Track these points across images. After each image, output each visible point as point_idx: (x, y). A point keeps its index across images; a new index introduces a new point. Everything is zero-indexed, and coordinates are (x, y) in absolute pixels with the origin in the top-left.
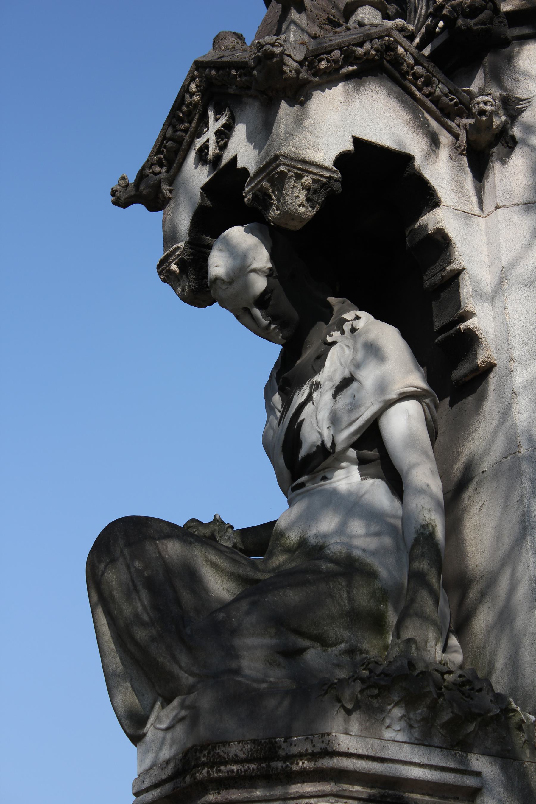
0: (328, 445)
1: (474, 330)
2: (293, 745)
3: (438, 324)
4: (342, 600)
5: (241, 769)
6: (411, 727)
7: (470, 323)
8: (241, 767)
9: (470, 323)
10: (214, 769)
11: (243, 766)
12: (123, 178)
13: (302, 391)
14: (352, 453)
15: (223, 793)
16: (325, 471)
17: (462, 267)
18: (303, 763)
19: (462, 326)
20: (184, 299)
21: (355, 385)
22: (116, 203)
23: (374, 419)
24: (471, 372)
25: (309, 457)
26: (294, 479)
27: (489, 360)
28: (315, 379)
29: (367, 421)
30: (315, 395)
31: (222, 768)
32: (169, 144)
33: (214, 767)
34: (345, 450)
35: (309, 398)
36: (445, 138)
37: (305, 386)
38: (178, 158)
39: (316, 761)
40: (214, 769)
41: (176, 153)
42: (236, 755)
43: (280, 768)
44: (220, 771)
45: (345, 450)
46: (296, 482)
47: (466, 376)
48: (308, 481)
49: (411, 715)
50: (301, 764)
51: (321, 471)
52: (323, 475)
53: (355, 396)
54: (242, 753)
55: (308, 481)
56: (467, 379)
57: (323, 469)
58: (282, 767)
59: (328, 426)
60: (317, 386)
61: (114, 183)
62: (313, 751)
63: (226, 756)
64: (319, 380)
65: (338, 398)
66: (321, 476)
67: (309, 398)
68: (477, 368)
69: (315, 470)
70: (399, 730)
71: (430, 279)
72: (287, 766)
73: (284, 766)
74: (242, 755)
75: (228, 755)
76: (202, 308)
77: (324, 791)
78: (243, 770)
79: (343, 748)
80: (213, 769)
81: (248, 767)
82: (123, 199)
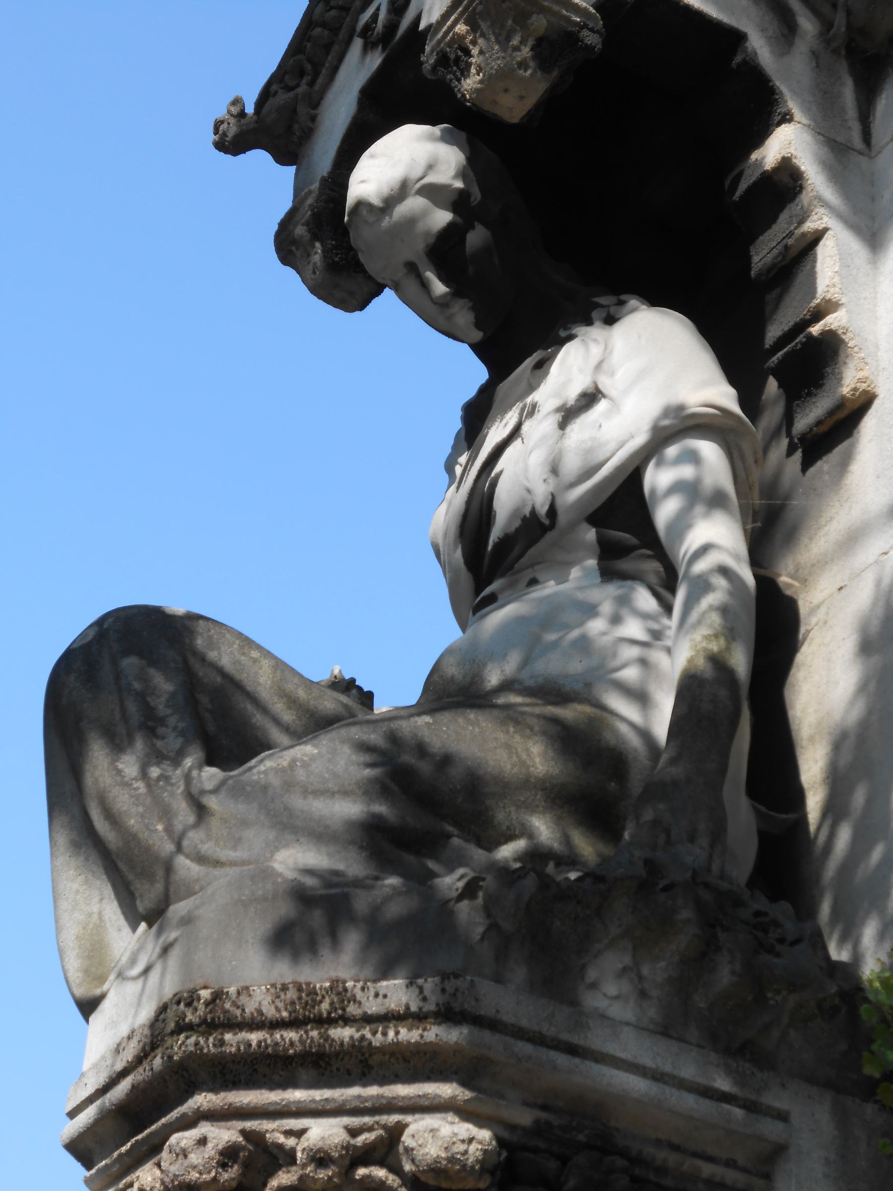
0: (543, 510)
1: (840, 332)
2: (381, 996)
3: (773, 332)
4: (528, 755)
5: (265, 1040)
6: (643, 994)
7: (832, 321)
8: (267, 1036)
9: (832, 321)
10: (211, 1040)
11: (271, 1035)
12: (237, 101)
13: (504, 421)
14: (591, 534)
15: (222, 1095)
16: (536, 568)
17: (823, 226)
18: (397, 1033)
19: (815, 330)
20: (317, 290)
21: (602, 406)
22: (221, 146)
23: (634, 466)
24: (831, 413)
25: (506, 541)
26: (478, 590)
27: (863, 386)
28: (529, 400)
29: (619, 469)
30: (525, 428)
31: (228, 1037)
32: (318, 30)
33: (211, 1034)
34: (573, 526)
35: (516, 433)
36: (807, 24)
37: (510, 414)
38: (330, 58)
39: (424, 1029)
40: (211, 1040)
41: (327, 48)
42: (260, 1012)
43: (347, 1040)
44: (222, 1043)
45: (573, 526)
46: (483, 594)
47: (819, 423)
48: (503, 589)
49: (645, 970)
50: (391, 1034)
51: (527, 568)
52: (531, 576)
53: (600, 426)
54: (273, 1009)
55: (503, 589)
56: (824, 428)
57: (532, 565)
58: (352, 1038)
59: (545, 477)
60: (533, 410)
61: (221, 111)
62: (420, 1009)
63: (238, 1012)
64: (536, 399)
65: (569, 429)
66: (526, 580)
67: (516, 433)
68: (842, 403)
69: (517, 566)
70: (616, 998)
71: (763, 254)
72: (363, 1038)
73: (357, 1036)
74: (270, 1012)
75: (243, 1010)
76: (347, 311)
77: (437, 1096)
78: (269, 1041)
79: (486, 1009)
80: (207, 1039)
81: (282, 1036)
82: (235, 139)
